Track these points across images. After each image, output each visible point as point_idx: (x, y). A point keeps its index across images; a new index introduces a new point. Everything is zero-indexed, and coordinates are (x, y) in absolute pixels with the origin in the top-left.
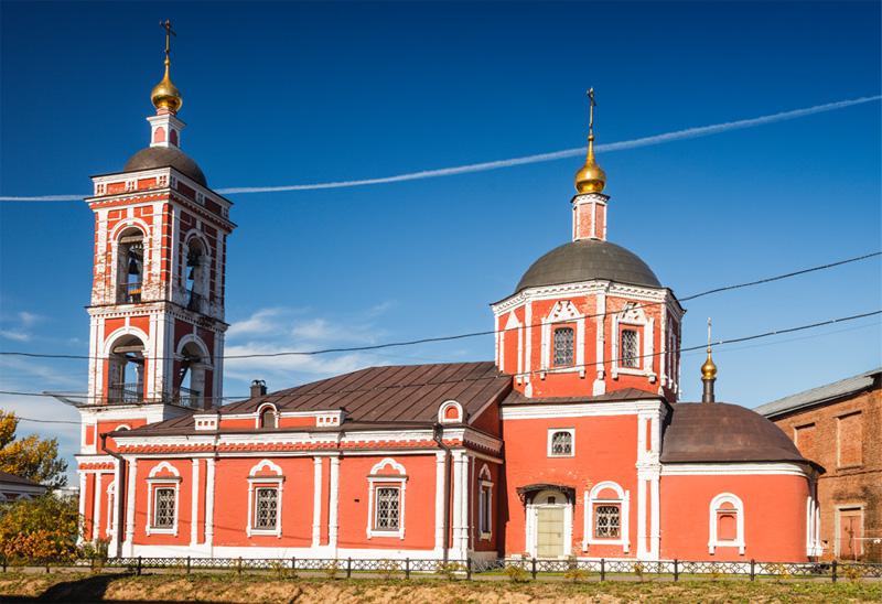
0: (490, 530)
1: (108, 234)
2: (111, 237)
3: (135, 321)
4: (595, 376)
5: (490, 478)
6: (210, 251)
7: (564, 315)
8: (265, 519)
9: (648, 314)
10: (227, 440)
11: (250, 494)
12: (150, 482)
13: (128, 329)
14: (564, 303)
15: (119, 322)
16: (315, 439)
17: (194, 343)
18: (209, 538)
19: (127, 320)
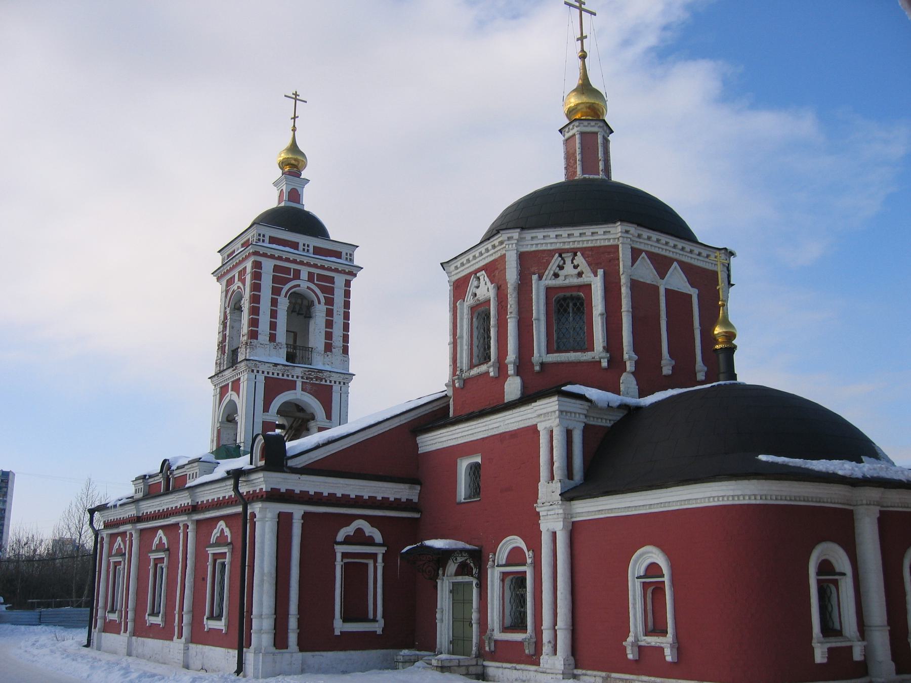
4: (506, 376)
6: (323, 300)
7: (568, 276)
14: (568, 257)
19: (299, 385)
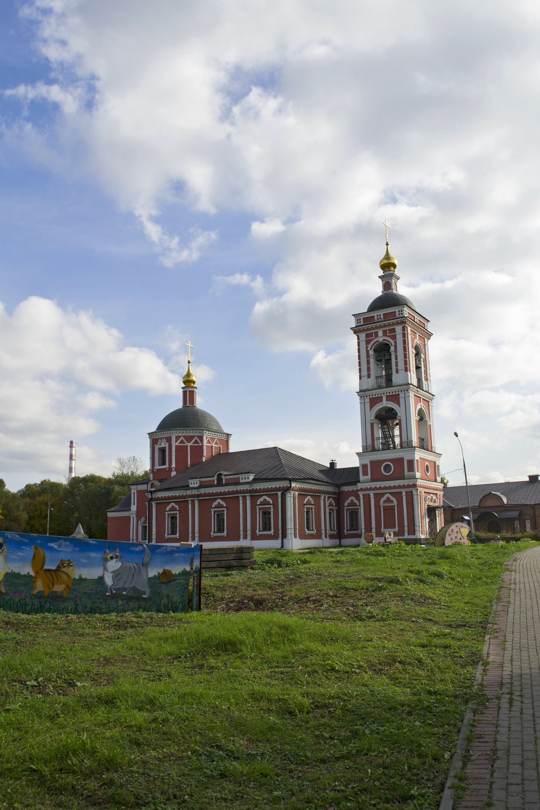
0: (335, 529)
1: (367, 347)
2: (369, 349)
3: (389, 398)
5: (334, 505)
7: (163, 445)
8: (220, 529)
10: (203, 491)
11: (167, 519)
12: (257, 507)
13: (385, 403)
15: (380, 399)
16: (189, 492)
18: (249, 537)
19: (384, 398)
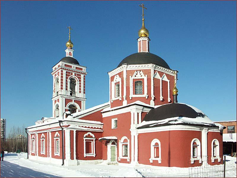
6: (78, 80)
7: (139, 77)
9: (145, 74)
12: (85, 139)
14: (139, 72)
17: (160, 80)
19: (73, 101)
